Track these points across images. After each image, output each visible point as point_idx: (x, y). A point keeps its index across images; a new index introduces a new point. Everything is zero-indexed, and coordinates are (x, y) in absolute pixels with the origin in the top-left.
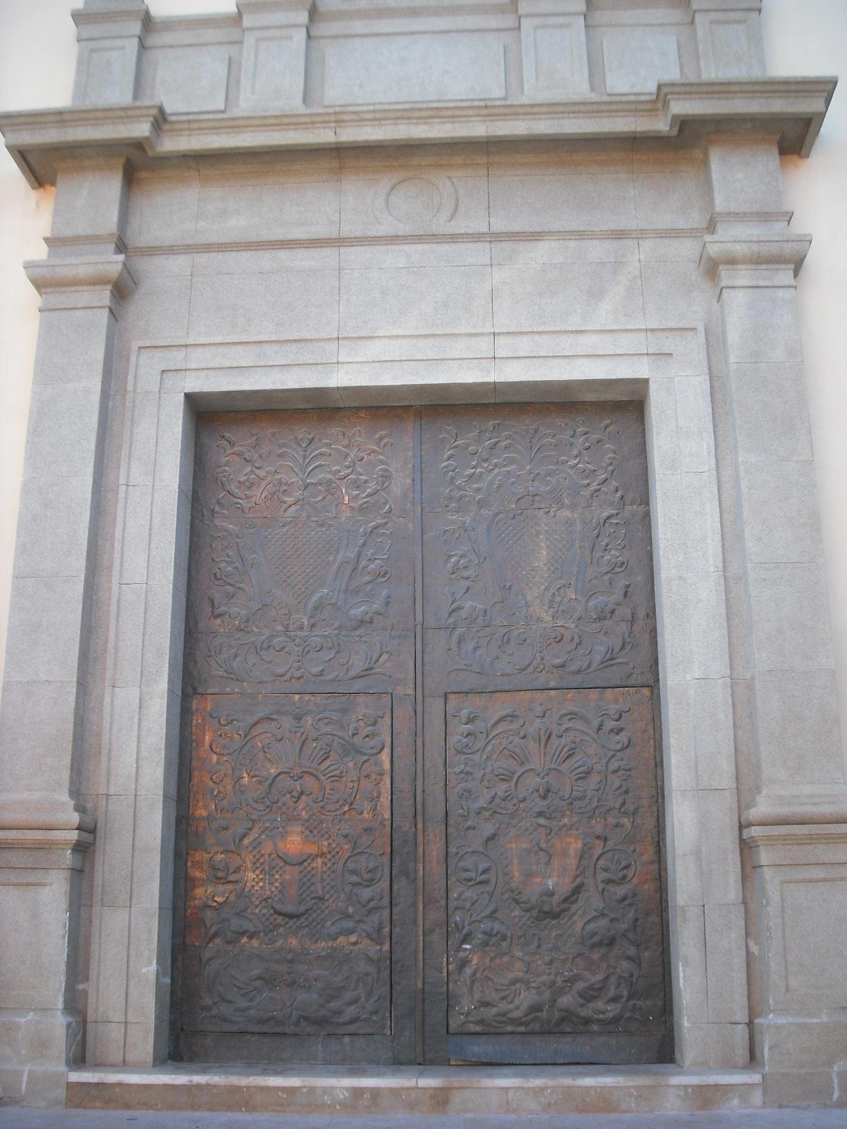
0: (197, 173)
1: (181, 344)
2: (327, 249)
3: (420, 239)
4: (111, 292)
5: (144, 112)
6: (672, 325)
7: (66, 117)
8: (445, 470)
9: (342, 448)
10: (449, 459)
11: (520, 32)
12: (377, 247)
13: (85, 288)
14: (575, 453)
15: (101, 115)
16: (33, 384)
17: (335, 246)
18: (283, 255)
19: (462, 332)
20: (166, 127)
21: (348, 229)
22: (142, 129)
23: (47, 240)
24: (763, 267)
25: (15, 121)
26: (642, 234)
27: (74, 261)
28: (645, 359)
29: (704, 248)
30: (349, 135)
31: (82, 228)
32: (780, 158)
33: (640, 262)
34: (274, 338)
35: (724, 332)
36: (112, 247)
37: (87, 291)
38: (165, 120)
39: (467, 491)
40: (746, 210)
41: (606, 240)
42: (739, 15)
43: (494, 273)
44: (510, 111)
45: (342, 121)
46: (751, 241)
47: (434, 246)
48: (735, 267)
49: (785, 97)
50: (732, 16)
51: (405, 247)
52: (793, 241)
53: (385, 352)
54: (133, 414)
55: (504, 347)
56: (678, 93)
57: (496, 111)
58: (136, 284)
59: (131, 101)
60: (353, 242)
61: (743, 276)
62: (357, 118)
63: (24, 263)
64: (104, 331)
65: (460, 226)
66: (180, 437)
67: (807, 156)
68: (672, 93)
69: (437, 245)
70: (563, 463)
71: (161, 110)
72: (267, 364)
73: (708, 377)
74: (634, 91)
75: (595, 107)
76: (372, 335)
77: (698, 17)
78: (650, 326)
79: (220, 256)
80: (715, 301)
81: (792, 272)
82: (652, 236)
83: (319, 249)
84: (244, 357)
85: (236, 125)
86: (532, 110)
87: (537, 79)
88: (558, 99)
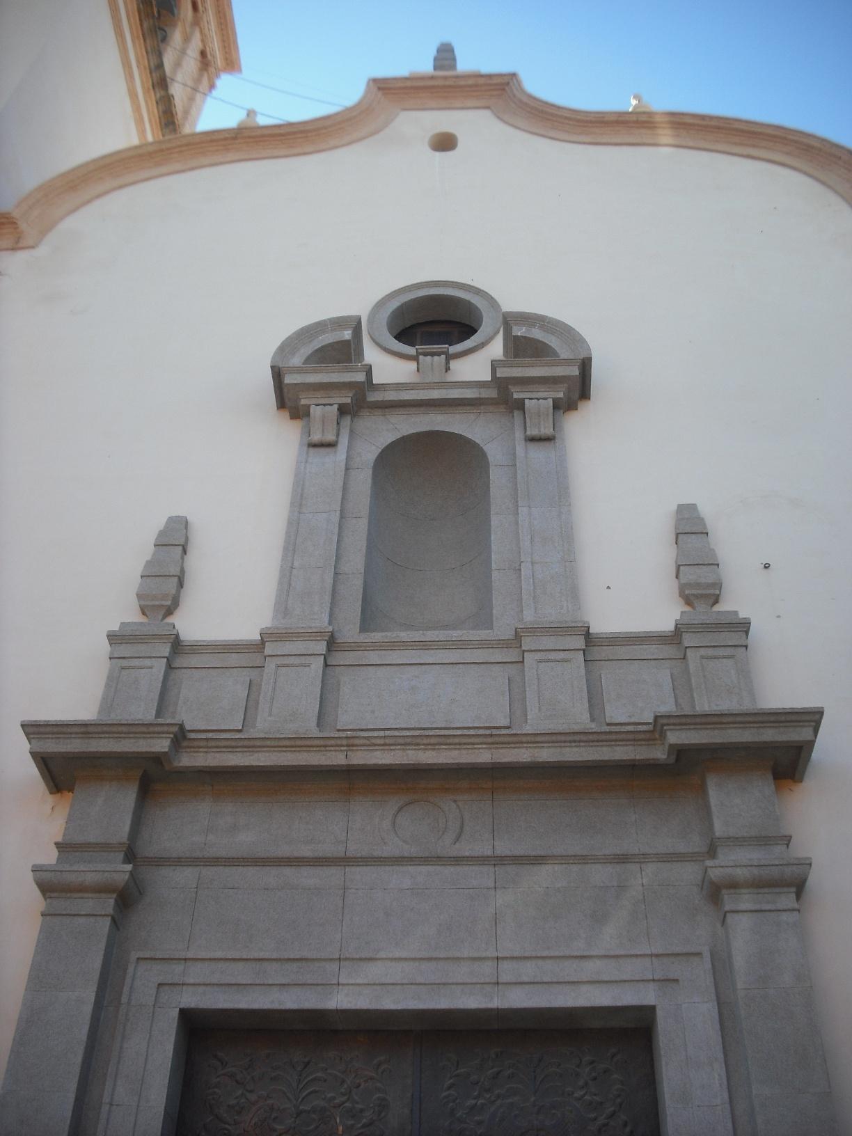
0: (211, 788)
1: (181, 957)
2: (332, 868)
3: (425, 861)
4: (116, 900)
5: (165, 729)
6: (677, 950)
7: (91, 729)
8: (445, 1100)
9: (338, 1073)
10: (449, 1088)
11: (524, 666)
12: (383, 867)
13: (90, 895)
14: (581, 1083)
15: (124, 729)
16: (26, 990)
17: (340, 866)
18: (288, 871)
19: (465, 956)
20: (185, 744)
21: (353, 849)
22: (161, 745)
23: (57, 844)
24: (766, 890)
25: (42, 729)
26: (644, 858)
27: (82, 868)
28: (651, 985)
29: (706, 872)
30: (360, 758)
31: (93, 836)
32: (775, 784)
33: (643, 885)
34: (275, 956)
35: (730, 956)
36: (121, 855)
37: (92, 898)
38: (185, 737)
39: (468, 1123)
40: (745, 835)
41: (608, 864)
42: (728, 651)
43: (497, 896)
44: (515, 739)
45: (353, 745)
46: (751, 866)
47: (439, 868)
48: (738, 891)
49: (776, 727)
50: (721, 652)
51: (410, 868)
52: (793, 864)
53: (387, 975)
54: (124, 1027)
55: (508, 972)
56: (674, 724)
57: (501, 739)
58: (141, 894)
59: (154, 717)
60: (359, 862)
61: (746, 901)
62: (368, 742)
63: (33, 867)
64: (104, 940)
65: (465, 849)
66: (170, 1054)
67: (801, 780)
68: (668, 725)
69: (443, 867)
70: (569, 1095)
71: (181, 726)
72: (266, 982)
73: (716, 1003)
74: (632, 720)
75: (595, 737)
76: (374, 956)
77: (689, 652)
78: (655, 951)
79: (227, 870)
80: (719, 925)
81: (794, 896)
82: (654, 860)
83: (325, 868)
84: (241, 974)
85: (252, 745)
86: (535, 739)
87: (540, 709)
88: (560, 729)
